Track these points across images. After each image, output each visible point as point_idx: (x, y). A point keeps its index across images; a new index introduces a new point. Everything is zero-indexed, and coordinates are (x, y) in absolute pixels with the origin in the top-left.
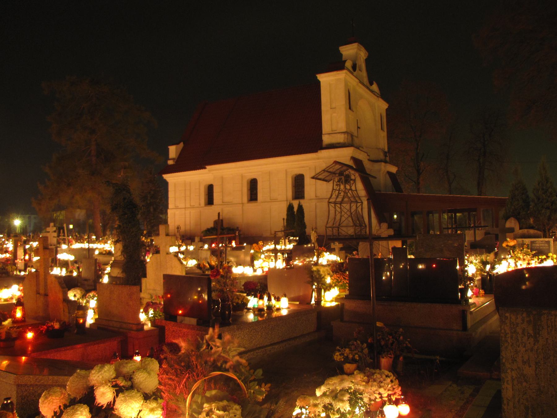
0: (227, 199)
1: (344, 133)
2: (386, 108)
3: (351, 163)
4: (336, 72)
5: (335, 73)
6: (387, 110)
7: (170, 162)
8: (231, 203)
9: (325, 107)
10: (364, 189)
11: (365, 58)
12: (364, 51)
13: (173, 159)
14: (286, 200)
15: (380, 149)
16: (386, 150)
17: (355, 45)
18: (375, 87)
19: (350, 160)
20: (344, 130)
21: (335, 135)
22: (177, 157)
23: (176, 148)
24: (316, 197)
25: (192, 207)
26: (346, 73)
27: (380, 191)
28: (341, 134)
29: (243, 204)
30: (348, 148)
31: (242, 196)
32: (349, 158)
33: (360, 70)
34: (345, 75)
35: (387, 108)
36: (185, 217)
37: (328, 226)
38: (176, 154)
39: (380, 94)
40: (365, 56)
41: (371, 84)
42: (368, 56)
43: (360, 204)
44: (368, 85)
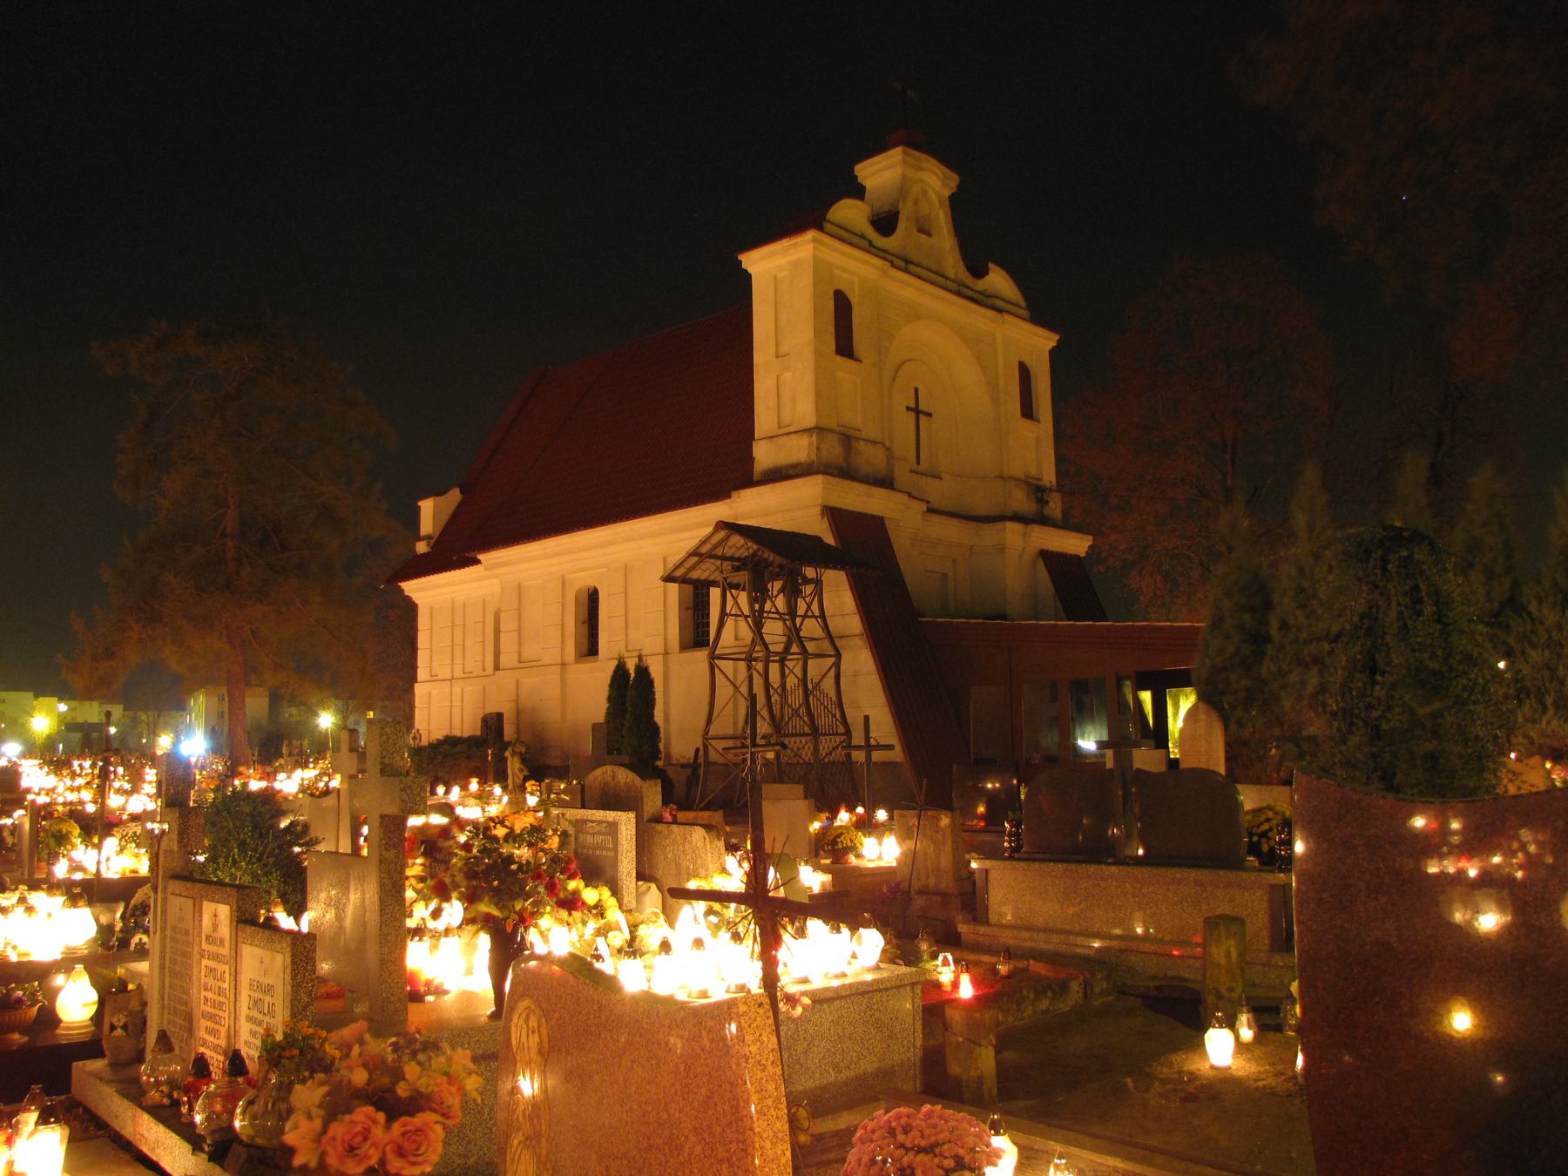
0: (530, 651)
1: (809, 430)
2: (1050, 347)
3: (821, 530)
4: (788, 239)
5: (785, 243)
6: (1052, 352)
7: (422, 548)
8: (537, 664)
9: (759, 358)
10: (856, 611)
11: (947, 193)
12: (939, 172)
13: (428, 538)
14: (662, 651)
15: (1012, 478)
16: (1049, 476)
17: (896, 154)
18: (998, 280)
19: (822, 518)
20: (810, 421)
21: (785, 438)
22: (438, 534)
23: (435, 506)
24: (737, 639)
25: (468, 676)
26: (814, 240)
27: (1004, 617)
28: (800, 434)
29: (563, 664)
30: (809, 478)
31: (563, 642)
32: (818, 510)
33: (924, 230)
34: (814, 248)
35: (1054, 347)
36: (451, 706)
37: (713, 731)
38: (434, 525)
39: (1022, 303)
40: (944, 185)
41: (979, 272)
42: (958, 186)
43: (833, 659)
44: (965, 276)
